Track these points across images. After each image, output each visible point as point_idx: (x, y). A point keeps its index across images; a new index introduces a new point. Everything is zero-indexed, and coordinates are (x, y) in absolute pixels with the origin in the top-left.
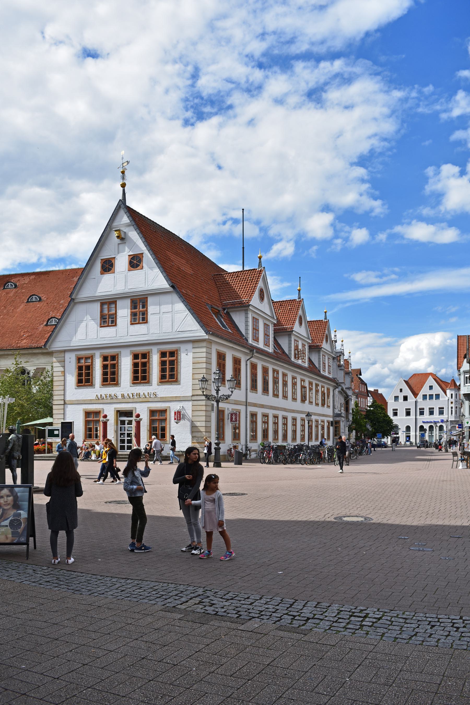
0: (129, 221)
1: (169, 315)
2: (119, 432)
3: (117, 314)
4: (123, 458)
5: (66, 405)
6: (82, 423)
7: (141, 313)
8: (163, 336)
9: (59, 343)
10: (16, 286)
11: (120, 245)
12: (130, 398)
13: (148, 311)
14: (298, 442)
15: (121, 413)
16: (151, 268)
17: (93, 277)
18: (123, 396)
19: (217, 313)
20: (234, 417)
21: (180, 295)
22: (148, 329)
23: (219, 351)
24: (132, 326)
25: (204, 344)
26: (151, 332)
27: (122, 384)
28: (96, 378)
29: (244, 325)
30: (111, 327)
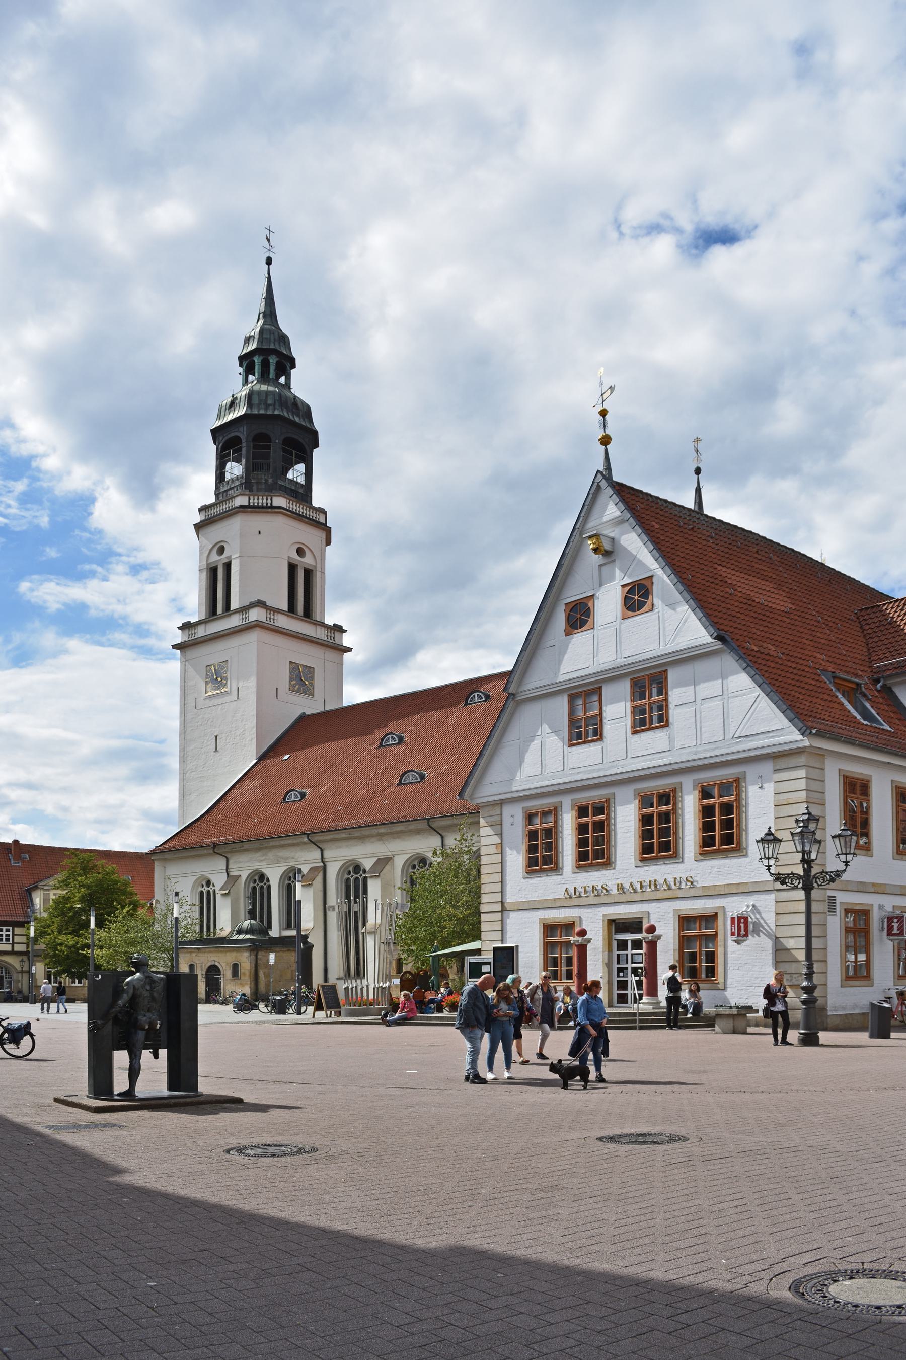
0: (618, 513)
1: (717, 703)
2: (615, 966)
3: (604, 714)
4: (653, 1021)
5: (505, 913)
6: (538, 949)
7: (655, 706)
8: (704, 750)
9: (489, 789)
10: (487, 697)
11: (603, 568)
12: (635, 891)
13: (670, 699)
15: (617, 926)
16: (672, 606)
17: (551, 643)
18: (620, 887)
19: (853, 692)
20: (896, 926)
21: (738, 655)
22: (671, 739)
23: (848, 774)
24: (635, 736)
25: (802, 760)
26: (678, 744)
27: (617, 863)
28: (565, 853)
30: (592, 744)
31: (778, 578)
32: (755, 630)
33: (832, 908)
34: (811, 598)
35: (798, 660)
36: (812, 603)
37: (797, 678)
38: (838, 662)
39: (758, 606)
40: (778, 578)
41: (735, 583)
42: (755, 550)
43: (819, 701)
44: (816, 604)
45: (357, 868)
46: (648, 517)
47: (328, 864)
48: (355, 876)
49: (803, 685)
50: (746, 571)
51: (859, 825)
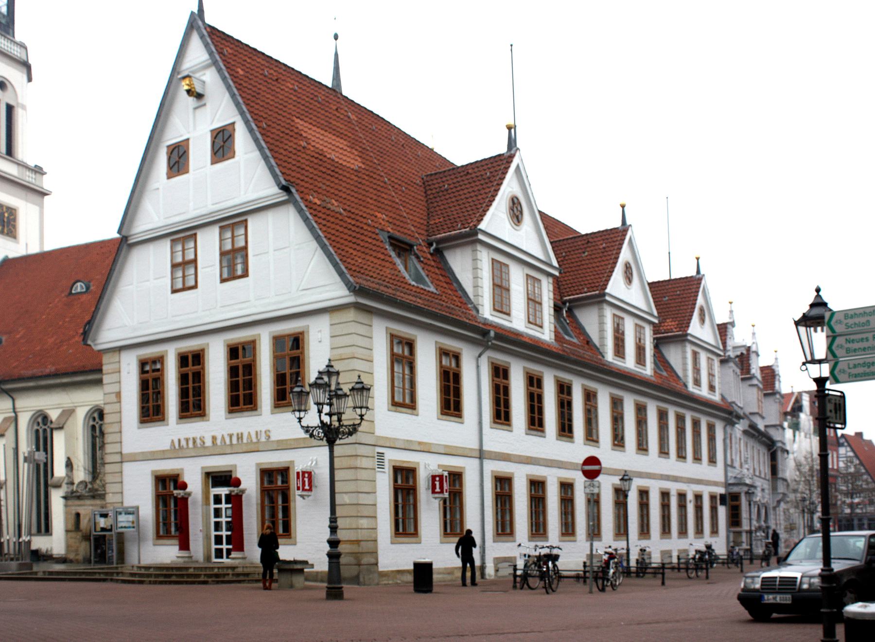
14: (608, 542)
29: (471, 276)
31: (353, 137)
32: (320, 185)
33: (381, 465)
34: (381, 159)
35: (358, 218)
36: (382, 164)
37: (354, 234)
38: (398, 223)
39: (329, 161)
40: (353, 137)
41: (309, 137)
42: (335, 108)
43: (372, 259)
44: (386, 166)
45: (46, 418)
46: (233, 63)
47: (20, 415)
48: (44, 427)
49: (359, 242)
50: (322, 127)
51: (452, 389)
